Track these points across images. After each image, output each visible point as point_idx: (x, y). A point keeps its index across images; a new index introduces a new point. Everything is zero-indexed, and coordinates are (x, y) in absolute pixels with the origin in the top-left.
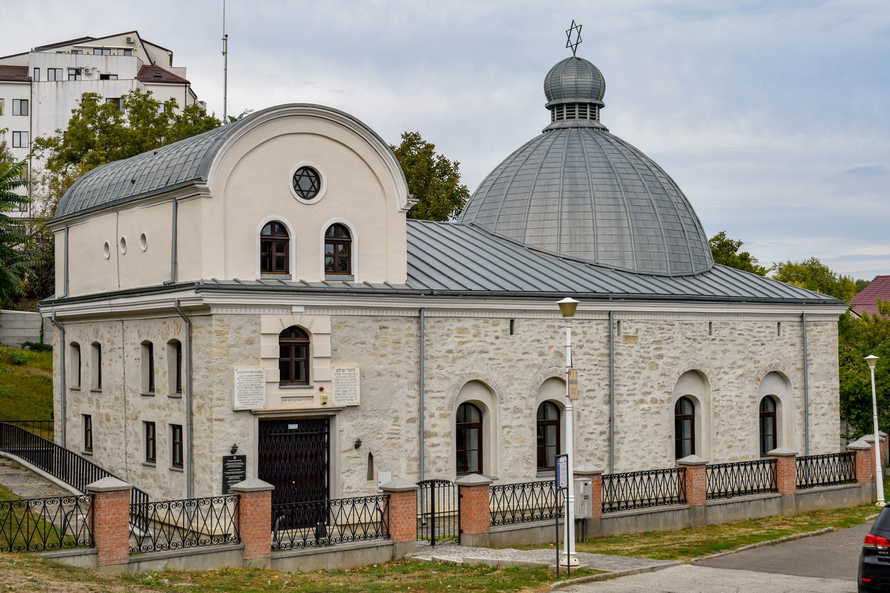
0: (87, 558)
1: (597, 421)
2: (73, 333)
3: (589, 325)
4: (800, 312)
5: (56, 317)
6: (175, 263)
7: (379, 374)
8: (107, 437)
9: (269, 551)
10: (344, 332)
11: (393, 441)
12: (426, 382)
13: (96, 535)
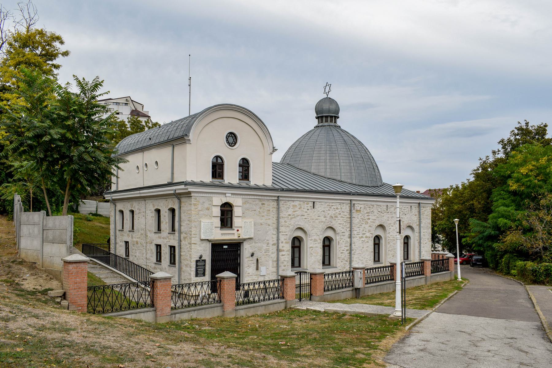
0: (150, 313)
2: (120, 206)
6: (173, 173)
9: (234, 306)
10: (247, 206)
12: (280, 228)
13: (155, 301)
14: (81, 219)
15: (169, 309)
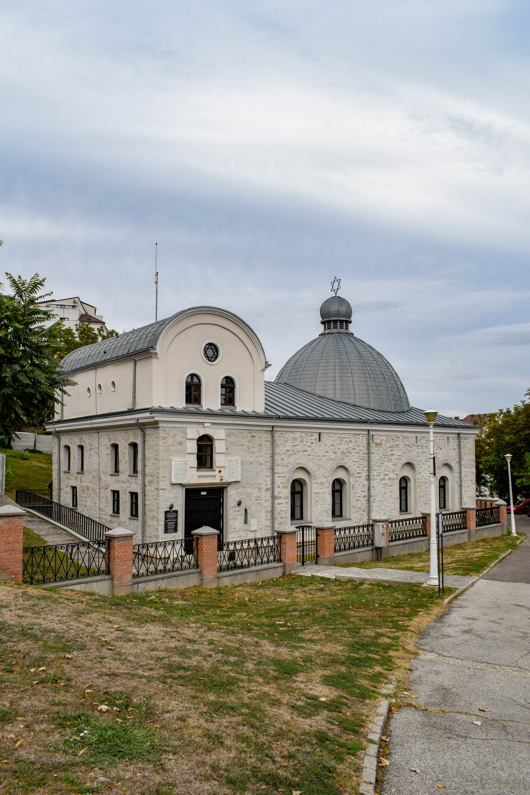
0: (106, 582)
1: (362, 490)
2: (65, 440)
3: (358, 437)
4: (458, 432)
5: (55, 431)
6: (134, 397)
7: (251, 463)
8: (87, 499)
10: (232, 439)
11: (258, 501)
12: (276, 467)
14: (14, 457)
15: (130, 577)
